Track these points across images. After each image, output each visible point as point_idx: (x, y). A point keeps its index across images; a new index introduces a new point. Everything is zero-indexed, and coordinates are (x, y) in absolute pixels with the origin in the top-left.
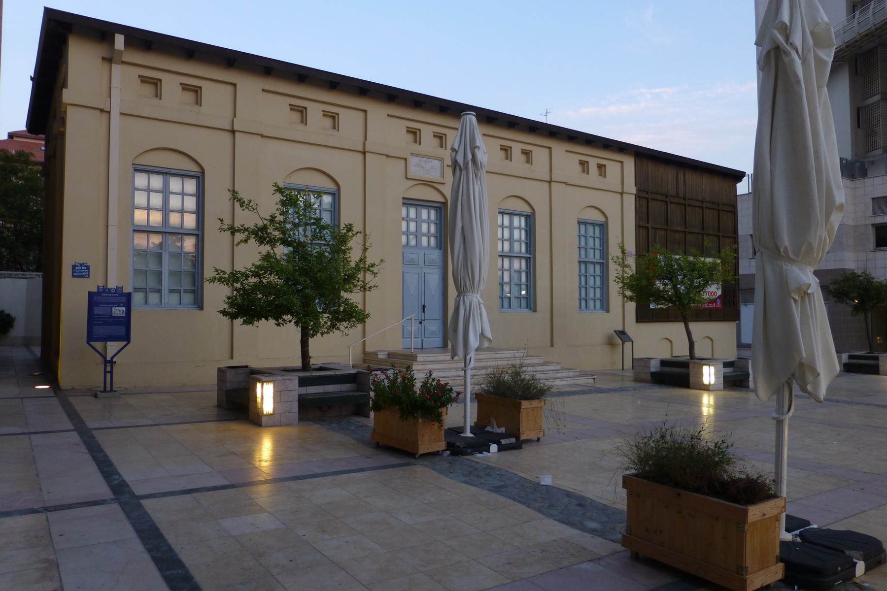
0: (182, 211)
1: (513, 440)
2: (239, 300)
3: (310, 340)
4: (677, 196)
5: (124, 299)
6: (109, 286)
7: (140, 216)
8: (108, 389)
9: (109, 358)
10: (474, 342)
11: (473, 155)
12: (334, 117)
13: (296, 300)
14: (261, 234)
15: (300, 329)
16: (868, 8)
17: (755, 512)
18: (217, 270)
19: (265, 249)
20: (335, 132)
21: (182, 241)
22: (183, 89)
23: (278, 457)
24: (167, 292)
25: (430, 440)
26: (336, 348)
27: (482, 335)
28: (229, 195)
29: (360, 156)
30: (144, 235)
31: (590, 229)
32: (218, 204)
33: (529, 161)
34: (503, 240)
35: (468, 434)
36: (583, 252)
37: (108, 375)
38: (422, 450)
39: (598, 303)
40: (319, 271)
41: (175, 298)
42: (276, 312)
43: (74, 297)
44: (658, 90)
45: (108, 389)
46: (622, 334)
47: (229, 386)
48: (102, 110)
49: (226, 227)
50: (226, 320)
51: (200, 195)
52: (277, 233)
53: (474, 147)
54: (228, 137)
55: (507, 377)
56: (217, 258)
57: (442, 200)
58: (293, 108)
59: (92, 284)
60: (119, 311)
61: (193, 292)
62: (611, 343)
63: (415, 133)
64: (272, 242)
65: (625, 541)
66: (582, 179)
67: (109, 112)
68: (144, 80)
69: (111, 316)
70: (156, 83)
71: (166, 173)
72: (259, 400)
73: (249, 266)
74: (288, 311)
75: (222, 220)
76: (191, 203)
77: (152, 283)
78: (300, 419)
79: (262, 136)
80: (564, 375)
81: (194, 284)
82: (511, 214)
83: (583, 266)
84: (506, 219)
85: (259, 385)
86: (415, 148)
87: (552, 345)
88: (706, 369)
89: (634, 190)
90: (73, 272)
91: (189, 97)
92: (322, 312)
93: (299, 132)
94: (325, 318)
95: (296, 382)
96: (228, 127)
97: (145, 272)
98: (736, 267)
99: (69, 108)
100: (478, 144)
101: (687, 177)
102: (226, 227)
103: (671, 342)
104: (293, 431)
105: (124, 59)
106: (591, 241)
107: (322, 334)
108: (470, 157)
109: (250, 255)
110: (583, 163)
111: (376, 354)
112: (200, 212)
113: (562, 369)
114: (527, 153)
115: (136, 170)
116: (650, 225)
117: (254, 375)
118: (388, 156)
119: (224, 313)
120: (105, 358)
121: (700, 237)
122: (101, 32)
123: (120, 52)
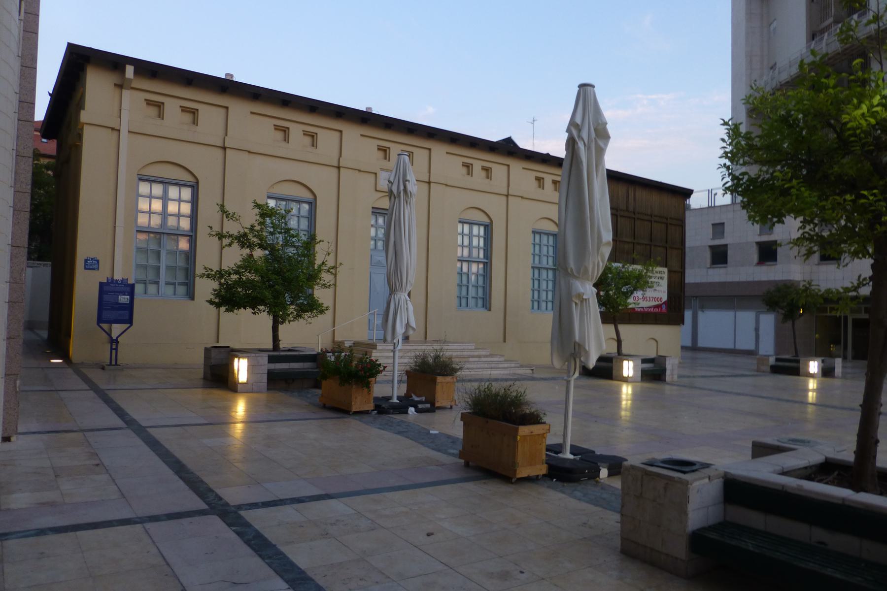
1: (428, 406)
2: (223, 292)
3: (280, 327)
5: (128, 289)
6: (115, 278)
7: (142, 220)
8: (113, 363)
9: (114, 338)
10: (400, 330)
11: (405, 186)
12: (313, 136)
13: (267, 294)
14: (242, 240)
15: (271, 317)
16: (822, 39)
17: (524, 430)
18: (205, 268)
19: (246, 251)
20: (313, 149)
21: (177, 242)
22: (182, 111)
23: (247, 411)
25: (360, 402)
26: (304, 335)
27: (408, 325)
28: (218, 208)
29: (336, 170)
31: (545, 238)
32: (209, 214)
33: (489, 177)
34: (462, 246)
35: (395, 400)
36: (537, 258)
37: (114, 352)
38: (354, 409)
39: (550, 305)
40: (288, 271)
41: (169, 290)
42: (252, 303)
43: (85, 288)
44: (654, 97)
45: (113, 363)
47: (213, 362)
48: (113, 129)
50: (213, 308)
51: (194, 202)
52: (255, 240)
53: (405, 181)
54: (220, 152)
55: (431, 360)
56: (209, 255)
58: (277, 128)
59: (102, 275)
60: (124, 299)
61: (186, 284)
63: (385, 151)
64: (251, 246)
65: (461, 455)
67: (119, 130)
68: (149, 103)
69: (118, 303)
70: (159, 106)
72: (236, 372)
73: (232, 266)
74: (262, 302)
76: (186, 208)
77: (151, 276)
78: (268, 389)
79: (249, 152)
80: (506, 365)
81: (187, 277)
82: (471, 224)
83: (536, 272)
84: (466, 227)
85: (236, 360)
86: (385, 163)
87: (505, 341)
88: (625, 363)
91: (188, 117)
92: (291, 304)
93: (282, 149)
94: (292, 309)
96: (221, 144)
97: (145, 267)
98: (683, 273)
99: (85, 127)
100: (408, 178)
101: (637, 194)
102: (214, 233)
104: (263, 396)
105: (133, 85)
106: (545, 249)
107: (289, 321)
108: (402, 188)
109: (234, 256)
110: (539, 180)
112: (194, 216)
113: (505, 361)
114: (487, 170)
115: (141, 180)
117: (233, 353)
118: (360, 171)
119: (211, 302)
120: (109, 335)
122: (114, 63)
123: (130, 80)
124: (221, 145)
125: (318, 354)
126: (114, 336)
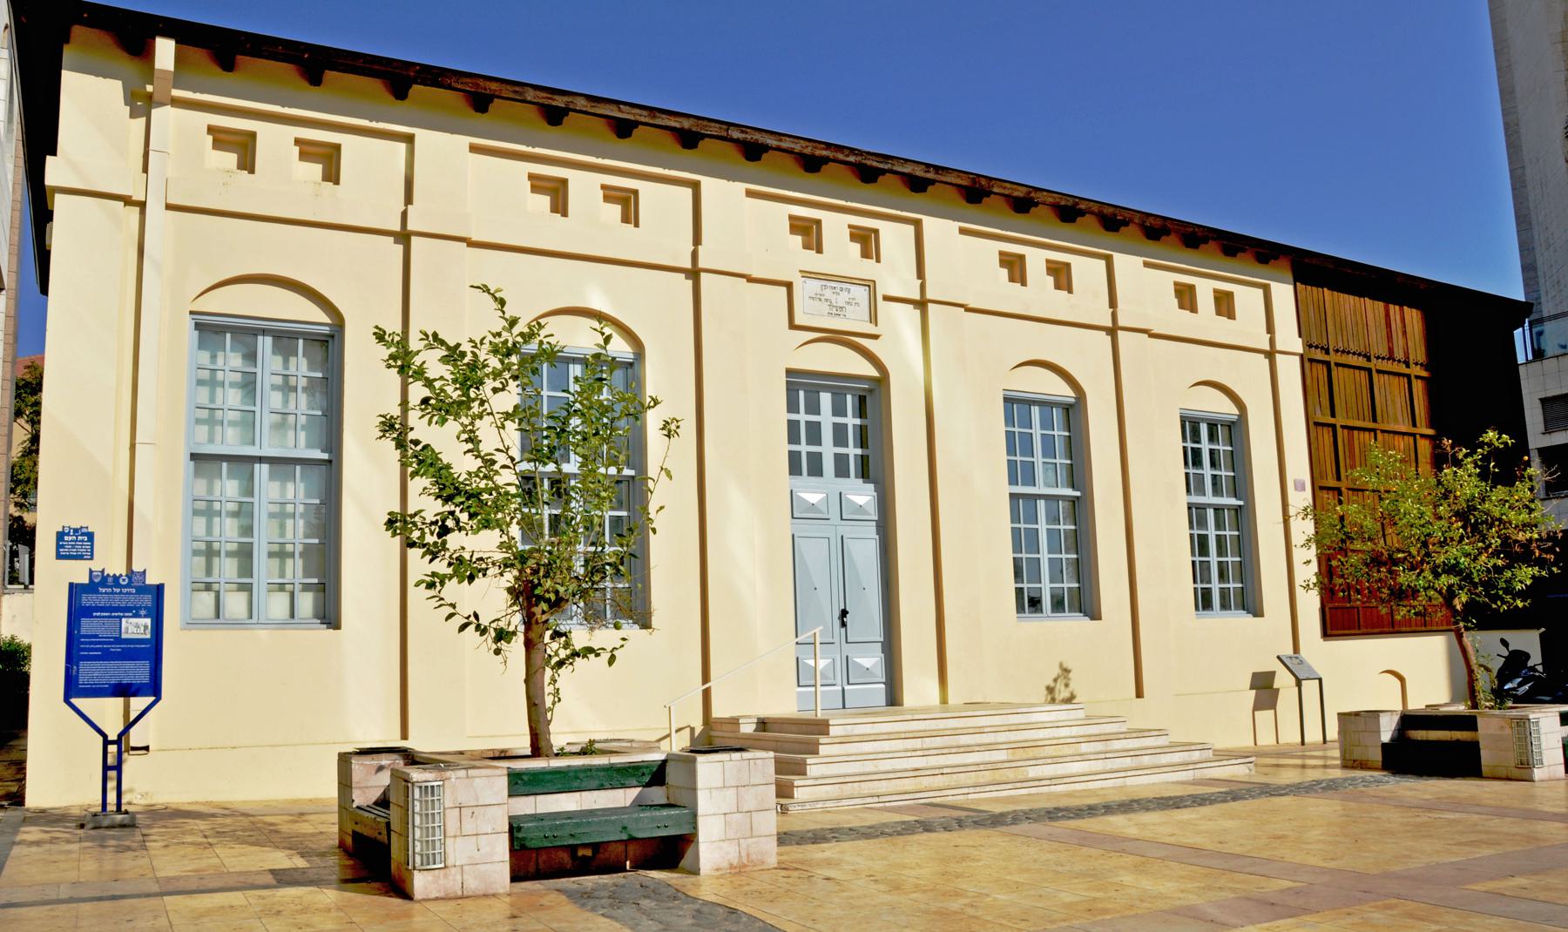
4: (1391, 358)
5: (147, 600)
24: (264, 587)
45: (111, 807)
48: (127, 201)
57: (874, 373)
60: (136, 628)
66: (1182, 323)
67: (142, 205)
69: (118, 640)
86: (811, 260)
90: (59, 547)
95: (771, 768)
99: (58, 198)
111: (734, 722)
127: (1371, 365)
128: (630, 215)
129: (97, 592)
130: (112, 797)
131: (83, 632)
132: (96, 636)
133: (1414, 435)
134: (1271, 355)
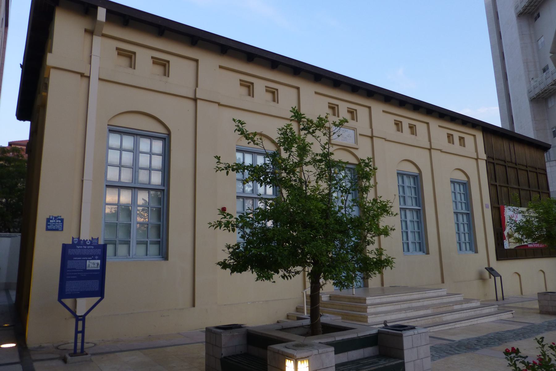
0: (150, 169)
4: (512, 162)
5: (99, 251)
6: (82, 238)
7: (112, 174)
8: (79, 351)
24: (135, 242)
30: (116, 191)
37: (80, 335)
41: (142, 248)
43: (47, 250)
45: (79, 351)
46: (491, 270)
47: (225, 352)
48: (82, 75)
49: (222, 166)
51: (166, 155)
54: (191, 104)
60: (93, 264)
61: (158, 243)
62: (482, 278)
68: (121, 52)
69: (85, 271)
70: (130, 56)
71: (137, 135)
75: (218, 158)
76: (157, 162)
77: (121, 235)
79: (219, 104)
89: (484, 157)
90: (47, 225)
91: (158, 70)
99: (52, 72)
102: (222, 166)
103: (519, 275)
112: (166, 170)
115: (111, 131)
116: (498, 184)
120: (74, 313)
121: (528, 192)
124: (192, 96)
125: (379, 333)
126: (80, 313)
127: (506, 164)
128: (275, 99)
129: (76, 248)
130: (79, 345)
131: (68, 267)
132: (75, 269)
133: (530, 190)
134: (477, 159)
